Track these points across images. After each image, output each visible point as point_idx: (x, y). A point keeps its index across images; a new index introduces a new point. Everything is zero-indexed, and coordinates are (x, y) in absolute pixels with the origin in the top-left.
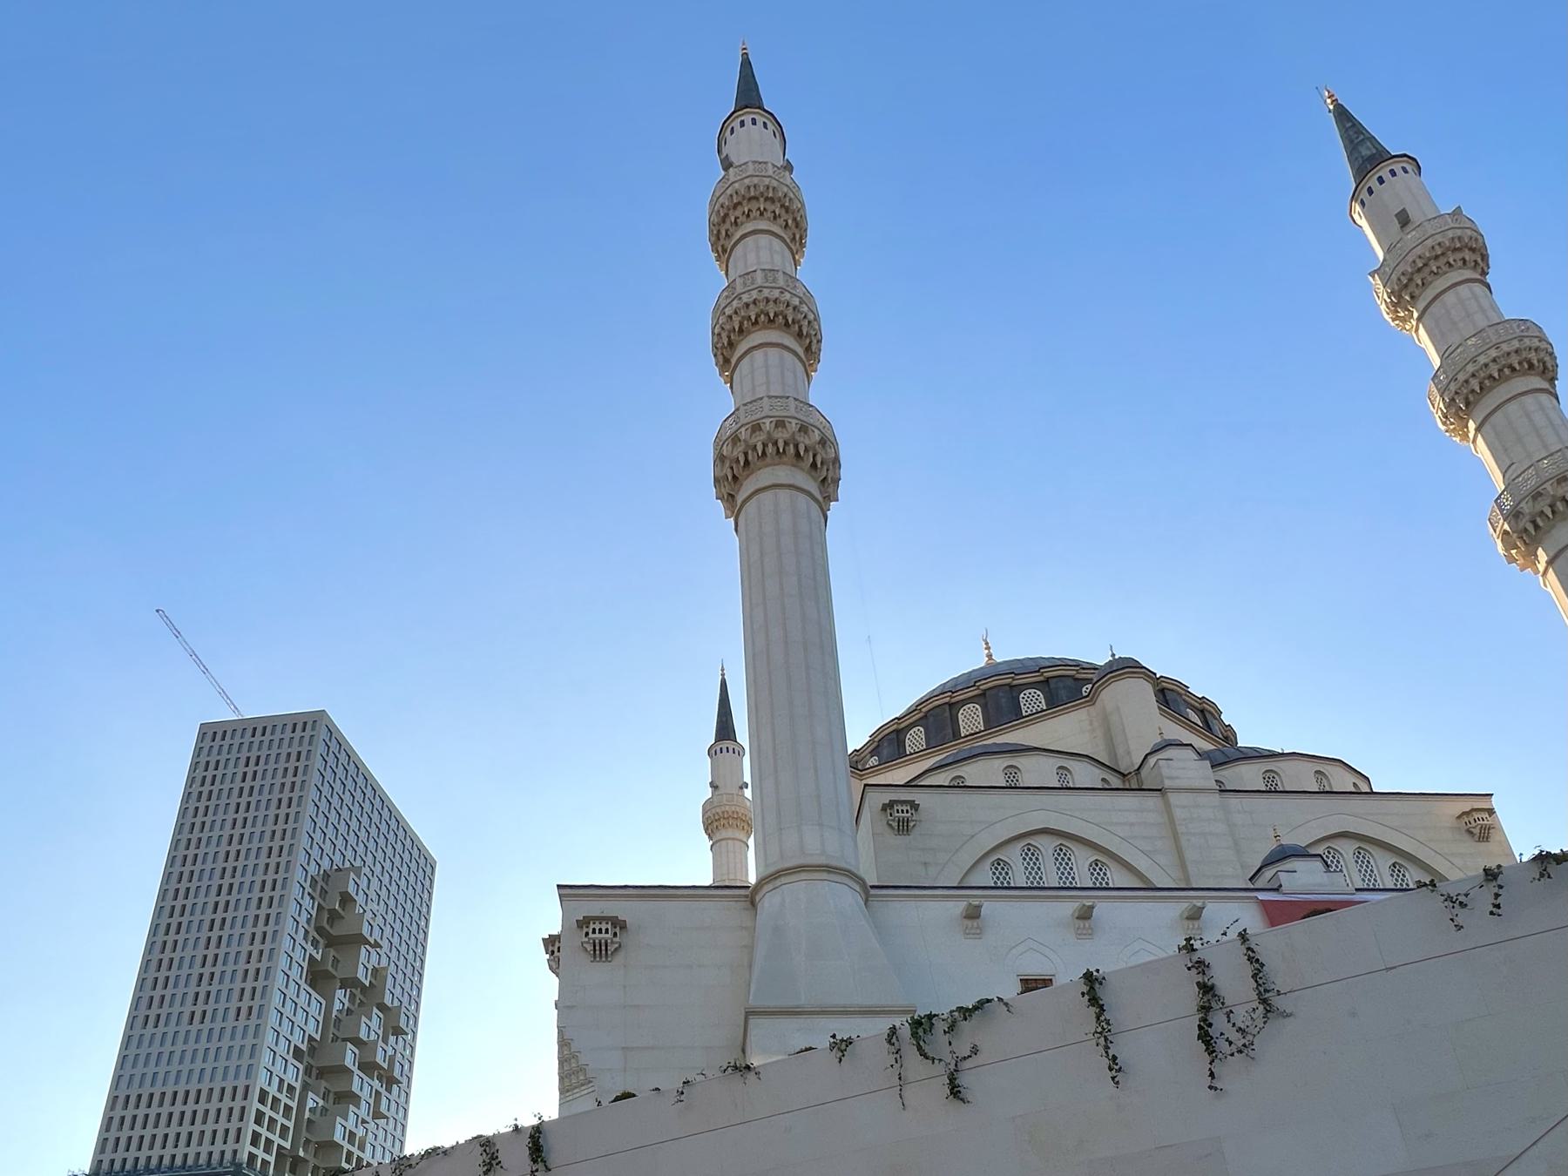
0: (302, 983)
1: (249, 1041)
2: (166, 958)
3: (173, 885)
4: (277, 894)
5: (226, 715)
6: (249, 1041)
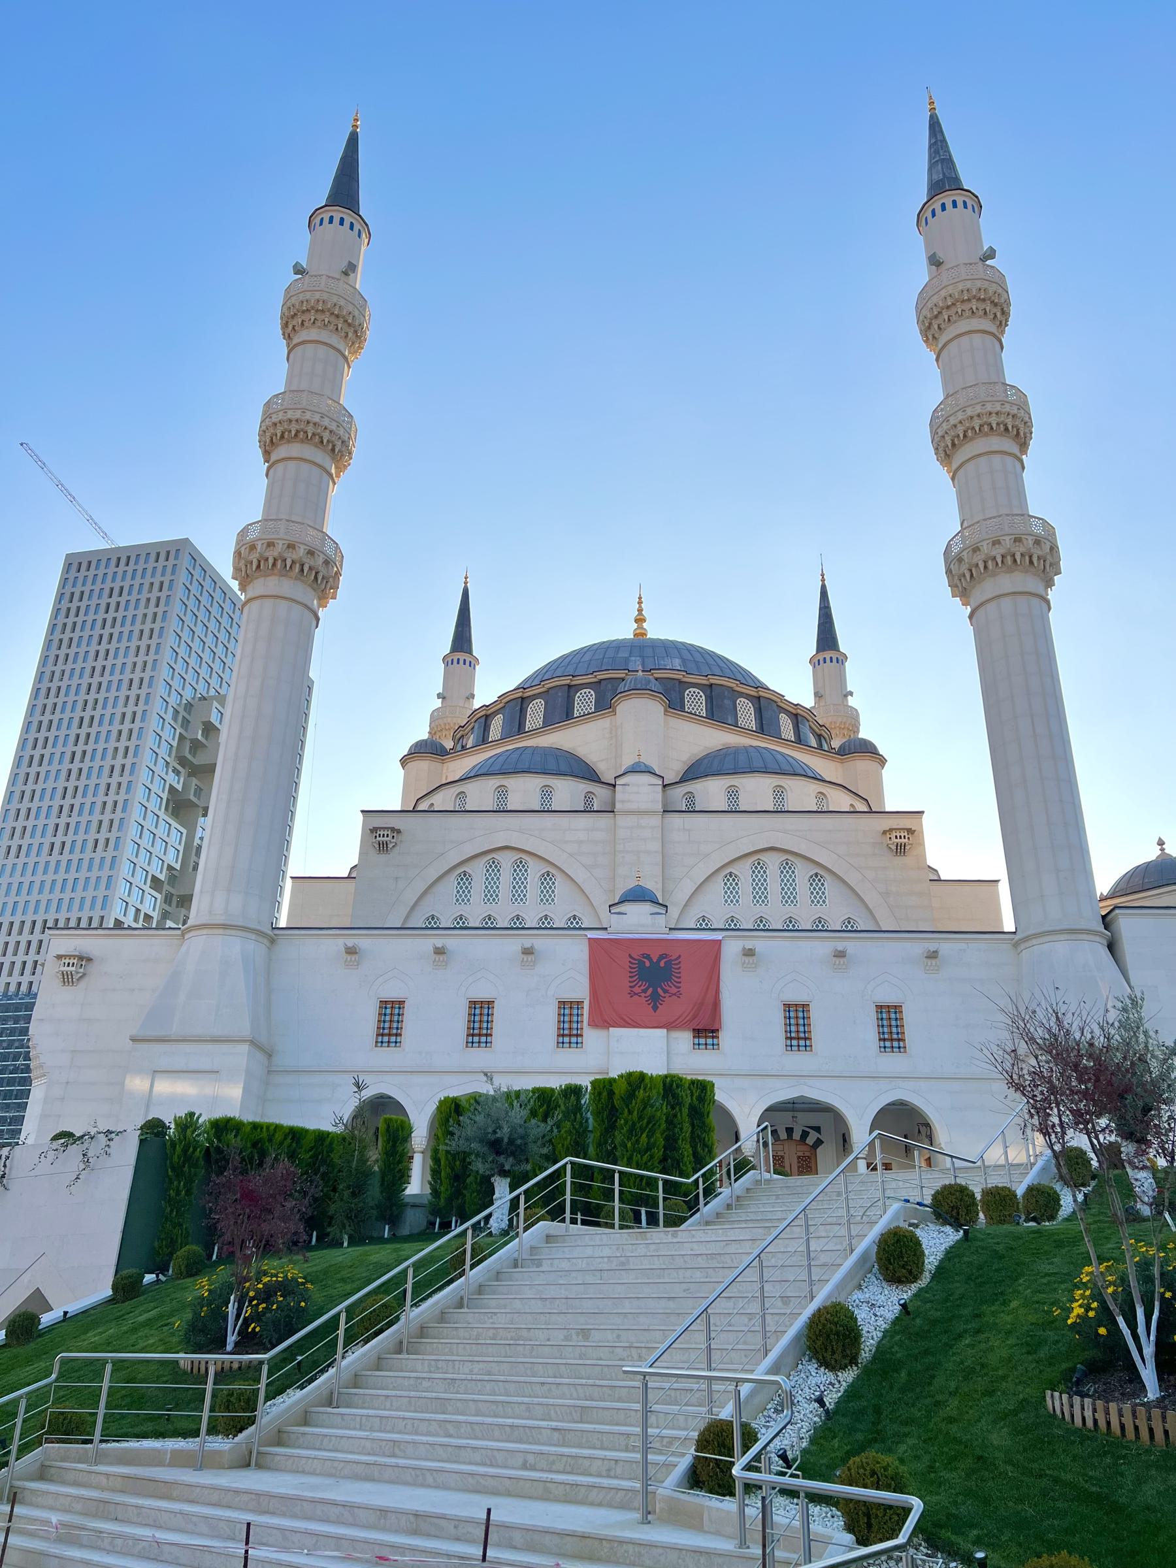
0: (162, 814)
1: (106, 872)
2: (37, 754)
3: (54, 651)
4: (157, 626)
5: (96, 544)
6: (106, 872)
